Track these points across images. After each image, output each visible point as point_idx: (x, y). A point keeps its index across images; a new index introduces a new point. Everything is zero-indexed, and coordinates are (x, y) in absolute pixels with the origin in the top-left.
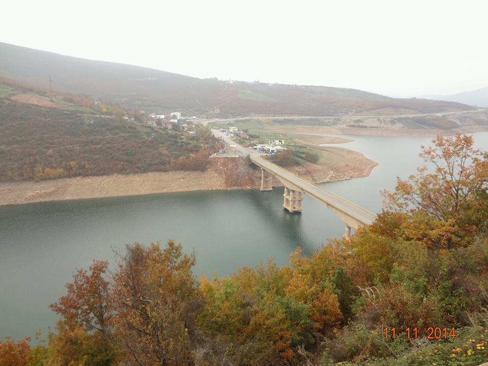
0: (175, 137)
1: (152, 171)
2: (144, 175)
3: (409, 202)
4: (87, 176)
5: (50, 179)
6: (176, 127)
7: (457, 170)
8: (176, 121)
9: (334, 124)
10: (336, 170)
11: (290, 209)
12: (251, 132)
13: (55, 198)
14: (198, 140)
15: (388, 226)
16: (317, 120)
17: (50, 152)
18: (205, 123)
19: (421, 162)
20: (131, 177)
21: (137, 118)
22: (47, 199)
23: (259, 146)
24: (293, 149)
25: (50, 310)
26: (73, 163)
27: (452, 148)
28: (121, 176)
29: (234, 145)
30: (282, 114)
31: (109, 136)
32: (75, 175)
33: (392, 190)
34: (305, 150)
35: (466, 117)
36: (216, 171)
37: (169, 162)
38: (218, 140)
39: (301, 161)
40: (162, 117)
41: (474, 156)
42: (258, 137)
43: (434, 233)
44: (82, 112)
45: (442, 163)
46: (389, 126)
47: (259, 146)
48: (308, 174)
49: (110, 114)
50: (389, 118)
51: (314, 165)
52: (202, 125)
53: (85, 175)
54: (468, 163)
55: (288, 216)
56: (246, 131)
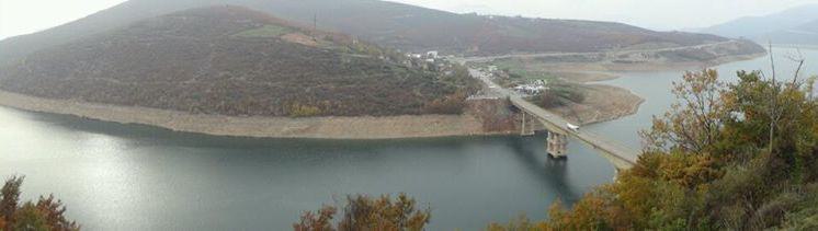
3: (667, 141)
5: (305, 116)
6: (431, 67)
8: (432, 60)
9: (600, 60)
10: (602, 109)
11: (554, 154)
12: (511, 71)
13: (307, 135)
15: (648, 168)
17: (308, 90)
18: (462, 62)
19: (673, 99)
20: (382, 119)
21: (392, 58)
23: (520, 87)
24: (557, 89)
25: (346, 197)
27: (701, 83)
29: (493, 86)
30: (545, 51)
33: (650, 131)
34: (567, 89)
37: (423, 105)
39: (566, 101)
40: (419, 56)
42: (519, 77)
43: (690, 170)
45: (692, 98)
46: (653, 59)
48: (573, 115)
50: (653, 52)
51: (580, 105)
52: (459, 64)
53: (337, 114)
54: (716, 95)
55: (552, 162)
56: (506, 71)
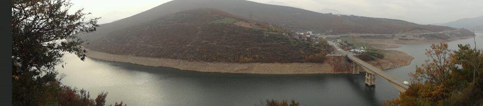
0: (308, 44)
1: (295, 62)
2: (291, 64)
3: (423, 78)
4: (263, 62)
5: (246, 62)
6: (309, 39)
7: (443, 61)
11: (369, 84)
12: (348, 42)
14: (320, 46)
16: (383, 36)
17: (247, 49)
20: (284, 65)
21: (289, 34)
22: (244, 72)
23: (353, 50)
26: (257, 56)
28: (279, 64)
29: (340, 50)
30: (366, 33)
31: (275, 43)
32: (257, 62)
33: (415, 73)
35: (452, 33)
36: (329, 63)
37: (304, 58)
38: (331, 46)
39: (375, 58)
40: (303, 34)
41: (449, 53)
42: (352, 45)
44: (264, 31)
45: (435, 57)
47: (353, 50)
48: (378, 65)
49: (277, 32)
50: (418, 34)
53: (262, 62)
54: (447, 56)
55: (368, 88)
